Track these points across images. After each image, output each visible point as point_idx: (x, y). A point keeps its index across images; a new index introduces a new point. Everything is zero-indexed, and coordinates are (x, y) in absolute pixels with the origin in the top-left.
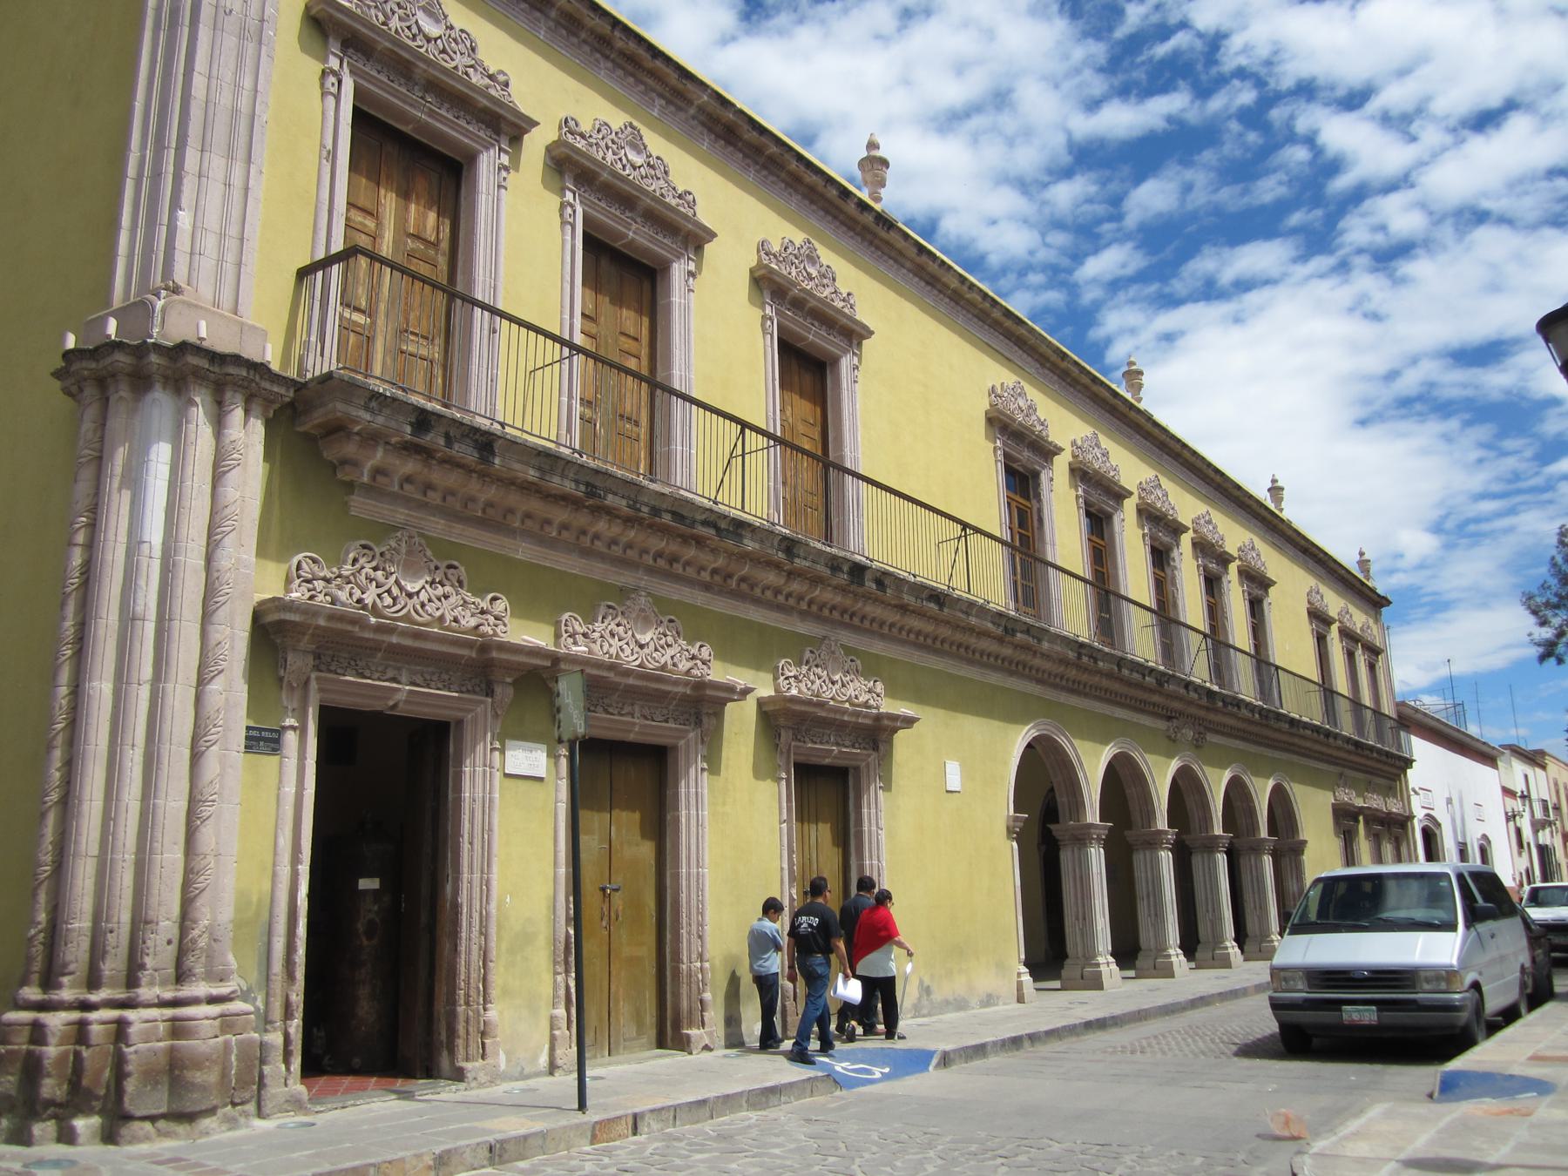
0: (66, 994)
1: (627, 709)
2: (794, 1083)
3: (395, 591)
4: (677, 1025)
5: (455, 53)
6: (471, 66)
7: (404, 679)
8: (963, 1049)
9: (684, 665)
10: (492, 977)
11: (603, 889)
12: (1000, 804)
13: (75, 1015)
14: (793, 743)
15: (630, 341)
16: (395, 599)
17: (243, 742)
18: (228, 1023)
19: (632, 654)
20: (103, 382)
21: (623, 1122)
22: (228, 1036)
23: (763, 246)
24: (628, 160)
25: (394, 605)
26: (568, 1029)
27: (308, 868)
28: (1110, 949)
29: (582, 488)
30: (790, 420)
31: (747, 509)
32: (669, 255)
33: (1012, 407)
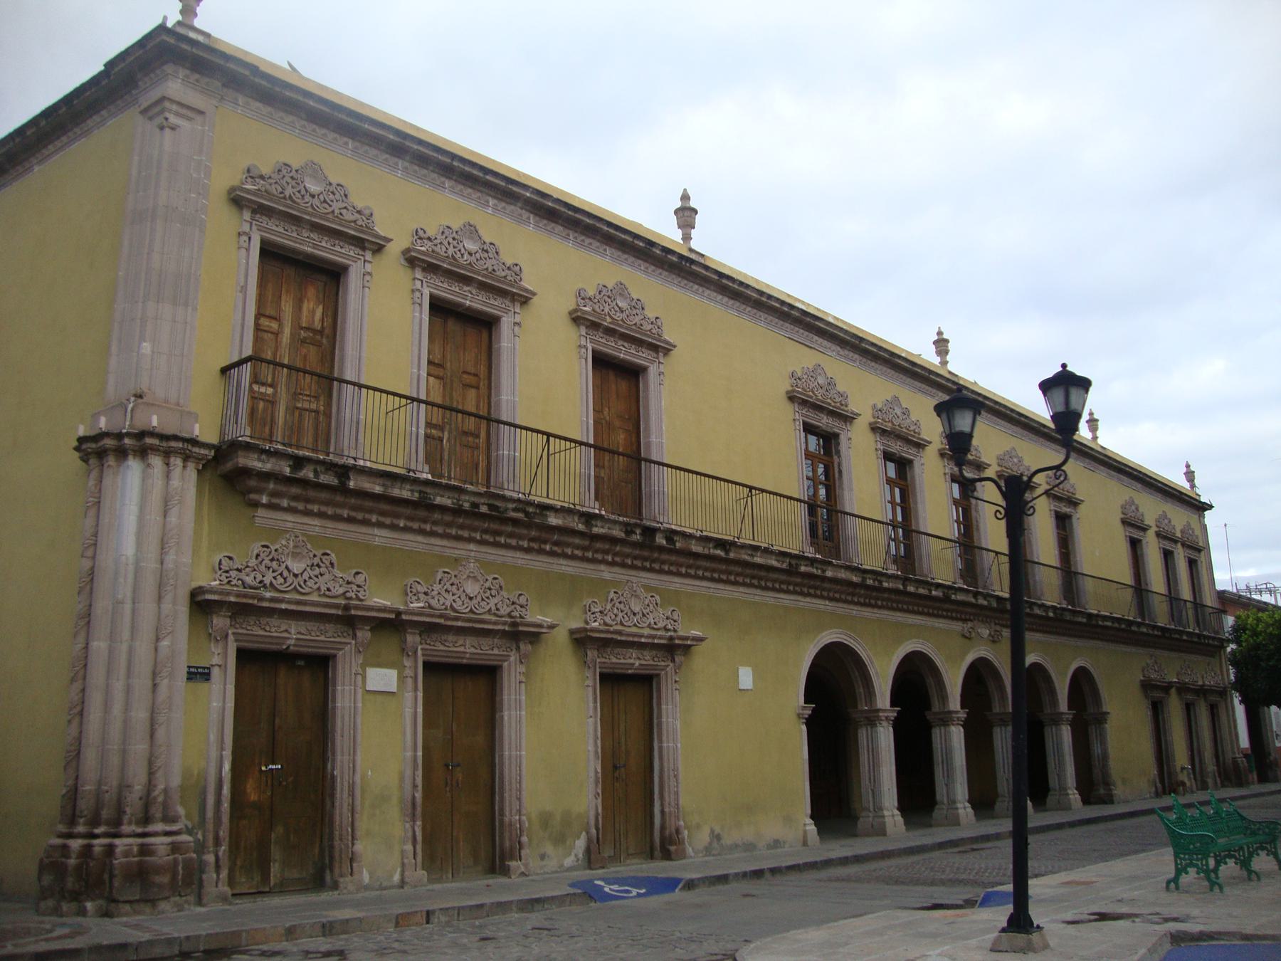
0: (81, 829)
1: (461, 642)
2: (555, 897)
3: (286, 573)
4: (503, 858)
5: (332, 201)
6: (345, 208)
7: (293, 631)
8: (706, 877)
9: (504, 610)
10: (357, 824)
11: (447, 766)
12: (795, 696)
13: (85, 842)
14: (598, 660)
15: (471, 377)
16: (285, 579)
17: (185, 676)
18: (175, 848)
19: (463, 604)
20: (101, 454)
21: (419, 914)
22: (176, 856)
23: (580, 294)
24: (465, 250)
26: (414, 858)
27: (230, 753)
29: (417, 495)
30: (608, 418)
32: (499, 313)
33: (812, 386)
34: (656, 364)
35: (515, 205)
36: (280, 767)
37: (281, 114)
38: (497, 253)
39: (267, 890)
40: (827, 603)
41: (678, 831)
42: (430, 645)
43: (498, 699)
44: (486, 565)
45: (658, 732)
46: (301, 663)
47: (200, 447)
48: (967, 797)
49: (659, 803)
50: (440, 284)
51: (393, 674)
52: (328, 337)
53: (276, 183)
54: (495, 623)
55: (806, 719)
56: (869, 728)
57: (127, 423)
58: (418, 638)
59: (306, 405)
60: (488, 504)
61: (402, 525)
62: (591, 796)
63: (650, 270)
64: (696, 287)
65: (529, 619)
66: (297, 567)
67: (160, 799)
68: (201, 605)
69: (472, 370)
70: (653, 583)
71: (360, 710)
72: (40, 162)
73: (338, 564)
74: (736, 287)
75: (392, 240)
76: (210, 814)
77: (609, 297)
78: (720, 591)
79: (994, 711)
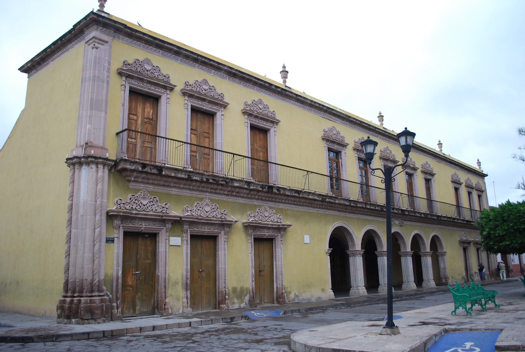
3: (141, 205)
4: (219, 305)
6: (159, 75)
7: (143, 225)
9: (219, 216)
10: (166, 292)
15: (207, 134)
16: (140, 206)
18: (102, 301)
20: (74, 164)
23: (246, 104)
25: (140, 208)
28: (364, 285)
29: (187, 176)
30: (256, 147)
34: (273, 128)
35: (221, 72)
37: (136, 42)
38: (215, 90)
40: (337, 212)
41: (282, 294)
42: (192, 229)
43: (217, 247)
44: (212, 201)
46: (147, 236)
50: (194, 101)
52: (155, 121)
53: (134, 66)
54: (216, 221)
57: (83, 153)
62: (250, 282)
64: (288, 100)
66: (145, 202)
67: (97, 284)
68: (110, 217)
69: (207, 131)
70: (273, 206)
76: (114, 289)
77: (256, 104)
79: (401, 251)
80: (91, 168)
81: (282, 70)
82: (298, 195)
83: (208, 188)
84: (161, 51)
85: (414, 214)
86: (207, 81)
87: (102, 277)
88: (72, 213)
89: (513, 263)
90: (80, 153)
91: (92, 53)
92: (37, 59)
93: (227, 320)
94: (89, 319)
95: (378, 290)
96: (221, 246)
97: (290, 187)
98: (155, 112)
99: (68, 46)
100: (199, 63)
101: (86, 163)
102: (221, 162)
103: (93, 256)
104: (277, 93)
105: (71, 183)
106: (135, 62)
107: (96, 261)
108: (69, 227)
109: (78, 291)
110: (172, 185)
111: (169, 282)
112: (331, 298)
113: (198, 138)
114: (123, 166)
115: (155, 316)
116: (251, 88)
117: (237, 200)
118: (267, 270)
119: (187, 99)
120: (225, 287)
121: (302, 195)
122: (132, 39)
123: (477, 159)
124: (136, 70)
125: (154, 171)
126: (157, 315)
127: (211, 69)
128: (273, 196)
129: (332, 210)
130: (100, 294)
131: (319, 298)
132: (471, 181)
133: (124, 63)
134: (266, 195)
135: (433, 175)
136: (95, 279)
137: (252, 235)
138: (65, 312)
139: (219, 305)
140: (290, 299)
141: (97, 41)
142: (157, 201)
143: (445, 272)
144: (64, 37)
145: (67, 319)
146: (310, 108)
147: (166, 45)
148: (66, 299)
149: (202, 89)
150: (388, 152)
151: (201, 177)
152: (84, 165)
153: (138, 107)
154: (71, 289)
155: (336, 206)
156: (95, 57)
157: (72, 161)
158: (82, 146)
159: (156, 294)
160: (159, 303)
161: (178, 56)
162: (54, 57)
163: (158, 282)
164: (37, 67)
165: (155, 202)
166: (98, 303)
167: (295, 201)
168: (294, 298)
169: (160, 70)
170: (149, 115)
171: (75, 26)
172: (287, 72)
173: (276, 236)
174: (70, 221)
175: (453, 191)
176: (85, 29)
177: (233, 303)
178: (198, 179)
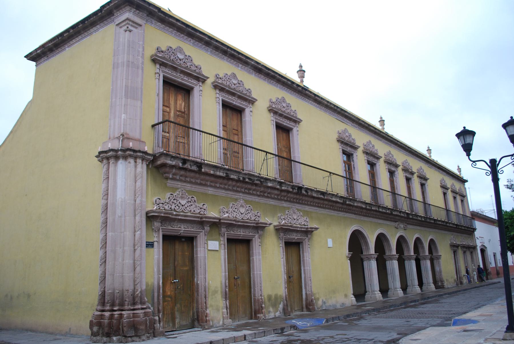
3: (179, 205)
4: (255, 314)
6: (192, 65)
7: (182, 227)
9: (253, 218)
10: (207, 302)
16: (179, 207)
18: (146, 314)
20: (108, 158)
22: (146, 317)
23: (270, 101)
29: (225, 174)
30: (280, 147)
31: (268, 175)
34: (296, 127)
35: (248, 67)
36: (178, 281)
37: (168, 28)
38: (243, 85)
39: (175, 330)
40: (353, 215)
41: (312, 301)
42: (229, 232)
43: (251, 252)
44: (246, 202)
45: (303, 263)
46: (183, 240)
47: (148, 155)
48: (400, 287)
49: (305, 290)
50: (225, 95)
51: (217, 243)
52: (187, 114)
53: (167, 54)
54: (251, 223)
55: (349, 258)
56: (368, 261)
57: (120, 146)
58: (225, 229)
59: (181, 141)
60: (248, 178)
61: (218, 186)
62: (284, 288)
63: (292, 93)
64: (307, 99)
65: (261, 221)
66: (183, 202)
67: (139, 295)
68: (150, 218)
69: (236, 128)
70: (299, 208)
71: (207, 257)
72: (68, 47)
73: (197, 201)
74: (320, 99)
75: (209, 78)
76: (156, 300)
77: (280, 102)
78: (321, 211)
79: (405, 255)
80: (129, 162)
81: (298, 69)
82: (323, 197)
83: (242, 188)
84: (192, 40)
85: (416, 218)
86: (235, 75)
87: (144, 287)
88: (107, 214)
89: (491, 266)
90: (117, 145)
91: (124, 37)
92: (50, 44)
93: (278, 331)
94: (133, 336)
95: (388, 294)
96: (256, 250)
97: (316, 188)
98: (187, 105)
99: (91, 30)
100: (228, 55)
101: (123, 157)
102: (252, 161)
103: (134, 263)
104: (297, 92)
105: (104, 179)
106: (168, 49)
107: (138, 269)
108: (104, 230)
109: (119, 304)
110: (209, 184)
111: (208, 290)
112: (354, 304)
113: (228, 134)
114: (163, 162)
115: (196, 329)
116: (275, 85)
117: (268, 202)
118: (295, 275)
119: (218, 93)
120: (261, 295)
121: (327, 196)
122: (164, 25)
123: (457, 166)
124: (170, 58)
125: (194, 168)
126: (198, 328)
127: (239, 63)
128: (301, 197)
129: (350, 213)
130: (143, 307)
131: (343, 304)
132: (455, 186)
133: (157, 49)
134: (295, 196)
135: (426, 179)
136: (137, 290)
137: (283, 239)
138: (103, 329)
139: (255, 314)
140: (319, 306)
141: (131, 23)
142: (195, 201)
143: (441, 275)
144: (87, 20)
145: (107, 337)
146: (325, 109)
147: (198, 34)
148: (103, 313)
149: (232, 83)
150: (391, 156)
151: (238, 175)
152: (121, 159)
153: (170, 99)
154: (110, 302)
155: (354, 209)
156: (129, 41)
157: (106, 155)
158: (118, 138)
159: (195, 305)
160: (200, 314)
161: (208, 47)
162: (71, 42)
163: (198, 291)
164: (48, 54)
165: (193, 202)
166: (142, 317)
167: (319, 203)
168: (322, 305)
169: (192, 60)
170: (181, 108)
171: (103, 7)
172: (304, 71)
173: (304, 240)
174: (105, 223)
175: (442, 195)
176: (115, 11)
177: (269, 312)
178: (235, 177)
